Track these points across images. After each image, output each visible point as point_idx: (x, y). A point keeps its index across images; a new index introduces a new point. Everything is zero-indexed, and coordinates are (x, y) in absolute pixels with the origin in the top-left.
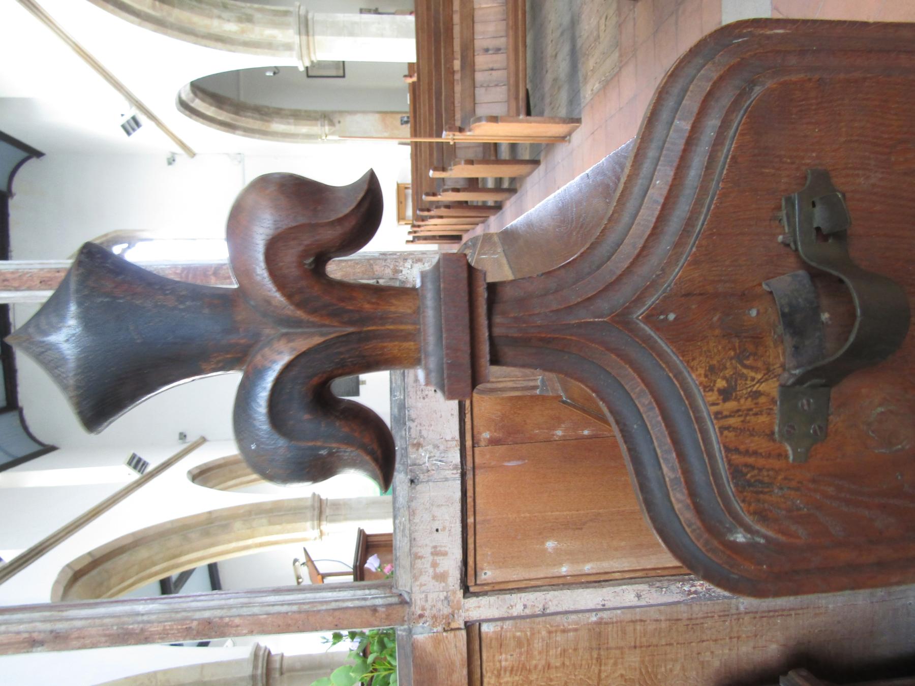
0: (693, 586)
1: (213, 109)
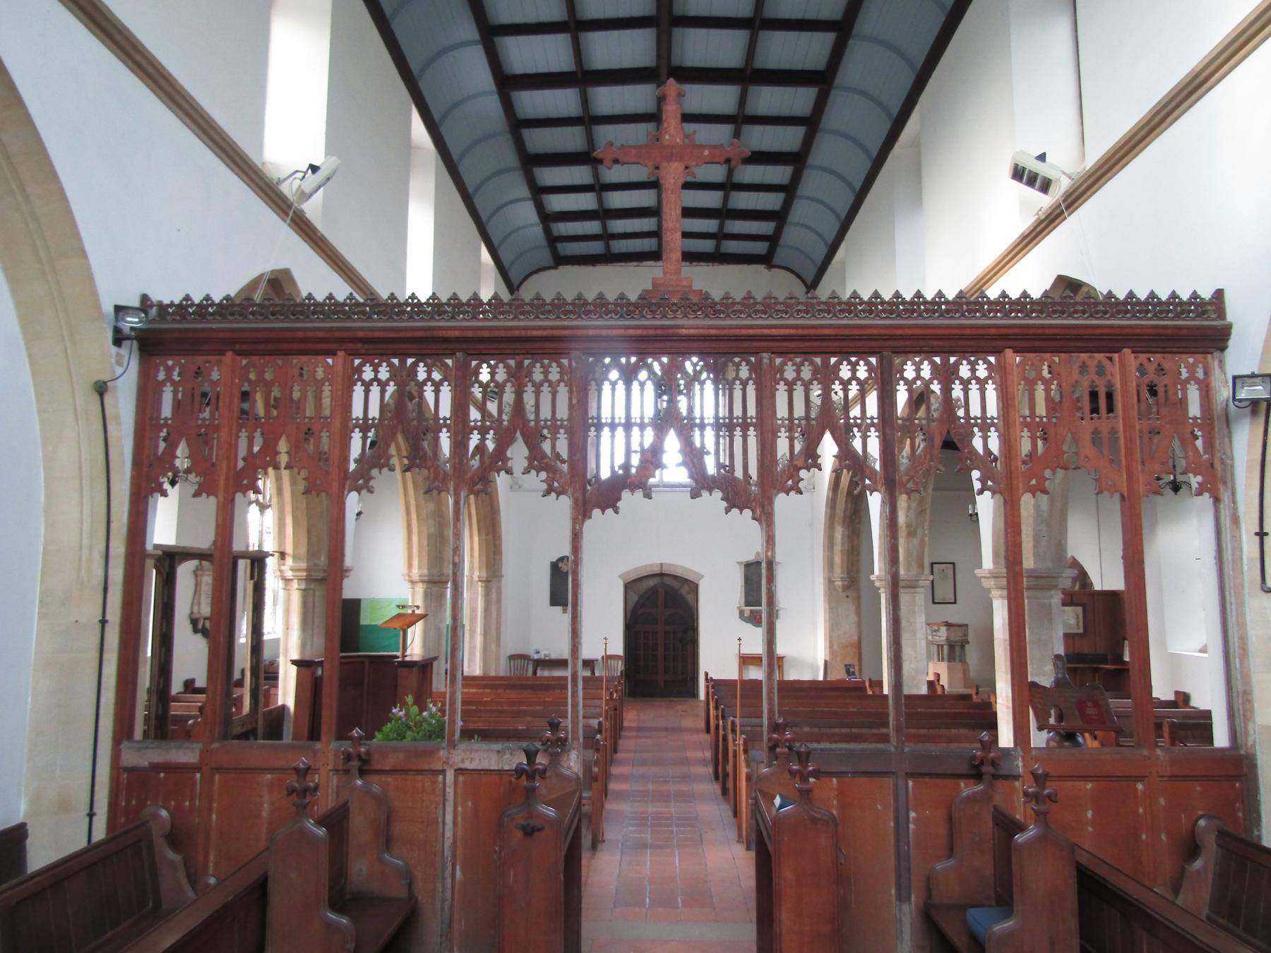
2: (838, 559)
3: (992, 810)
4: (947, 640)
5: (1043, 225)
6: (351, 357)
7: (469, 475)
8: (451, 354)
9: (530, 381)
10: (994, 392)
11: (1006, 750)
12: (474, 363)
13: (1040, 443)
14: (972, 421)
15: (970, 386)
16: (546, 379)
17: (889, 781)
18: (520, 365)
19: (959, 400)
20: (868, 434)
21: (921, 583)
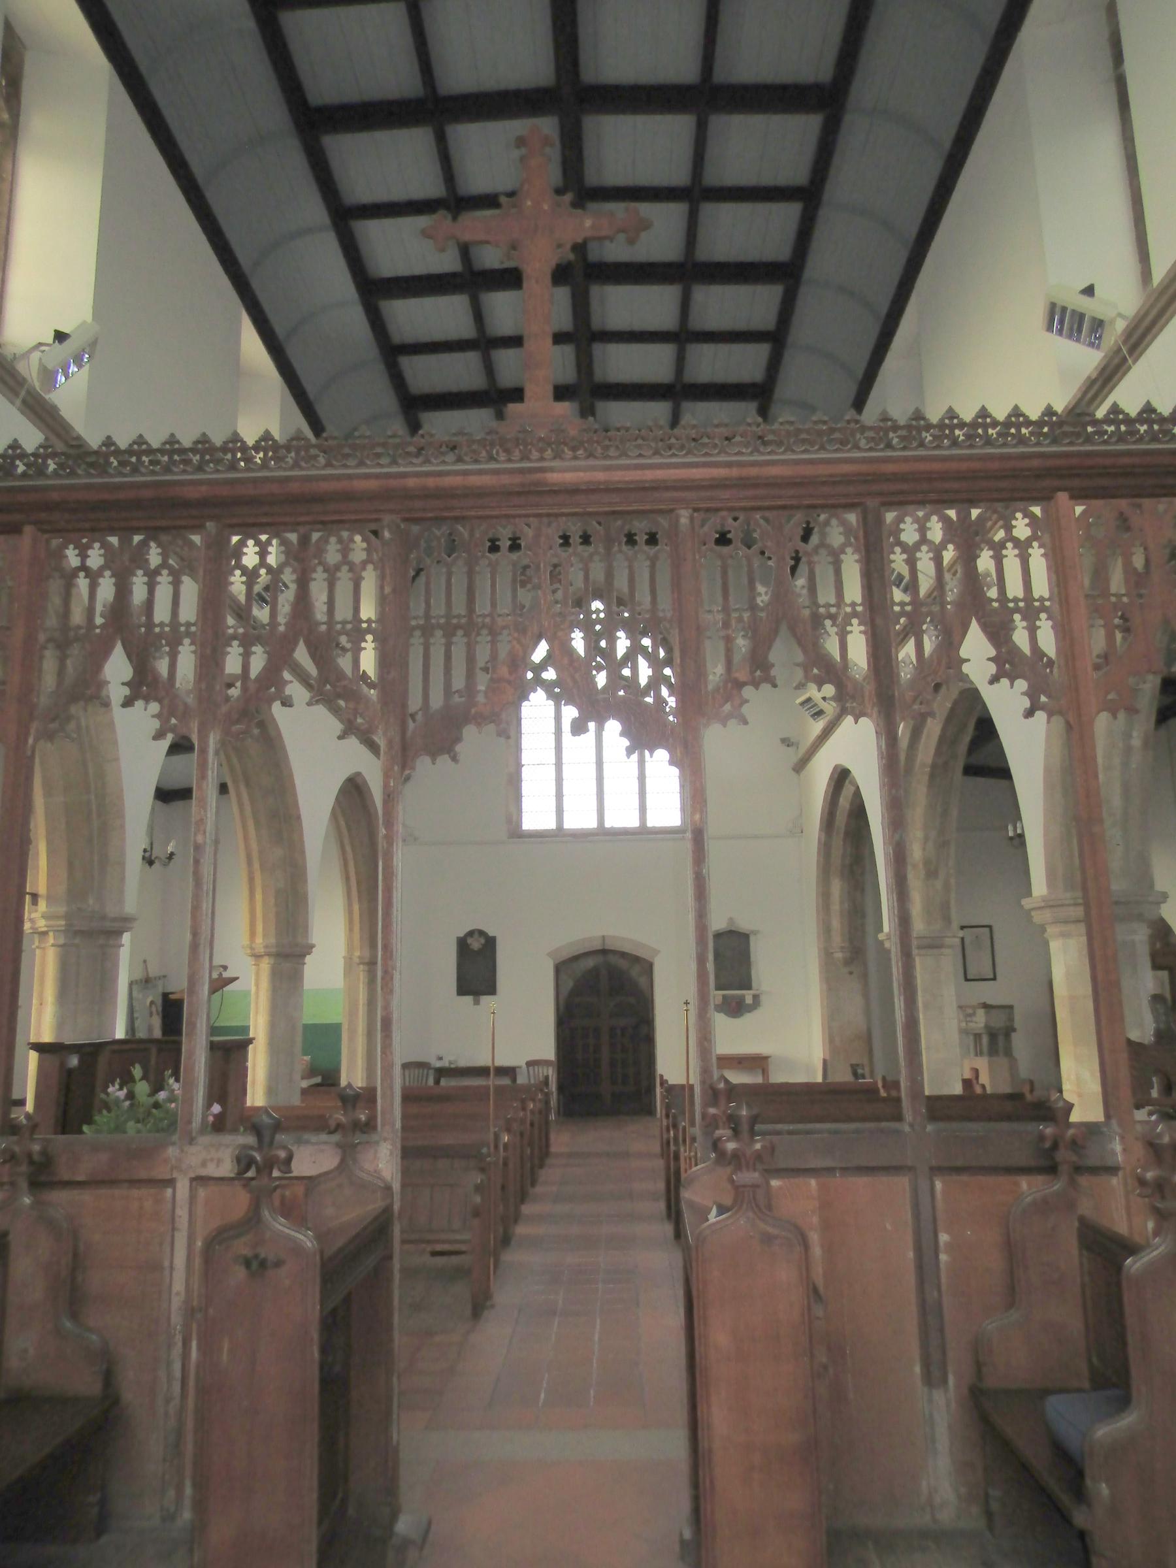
0: (179, 1332)
1: (848, 806)
2: (836, 923)
3: (1076, 1224)
4: (987, 1027)
5: (1096, 387)
6: (46, 536)
7: (224, 709)
8: (197, 528)
9: (320, 563)
10: (1043, 560)
11: (1091, 1129)
12: (235, 539)
13: (1119, 636)
14: (1011, 605)
15: (1004, 552)
16: (345, 560)
17: (903, 1182)
18: (304, 540)
19: (988, 574)
20: (849, 628)
21: (948, 941)
